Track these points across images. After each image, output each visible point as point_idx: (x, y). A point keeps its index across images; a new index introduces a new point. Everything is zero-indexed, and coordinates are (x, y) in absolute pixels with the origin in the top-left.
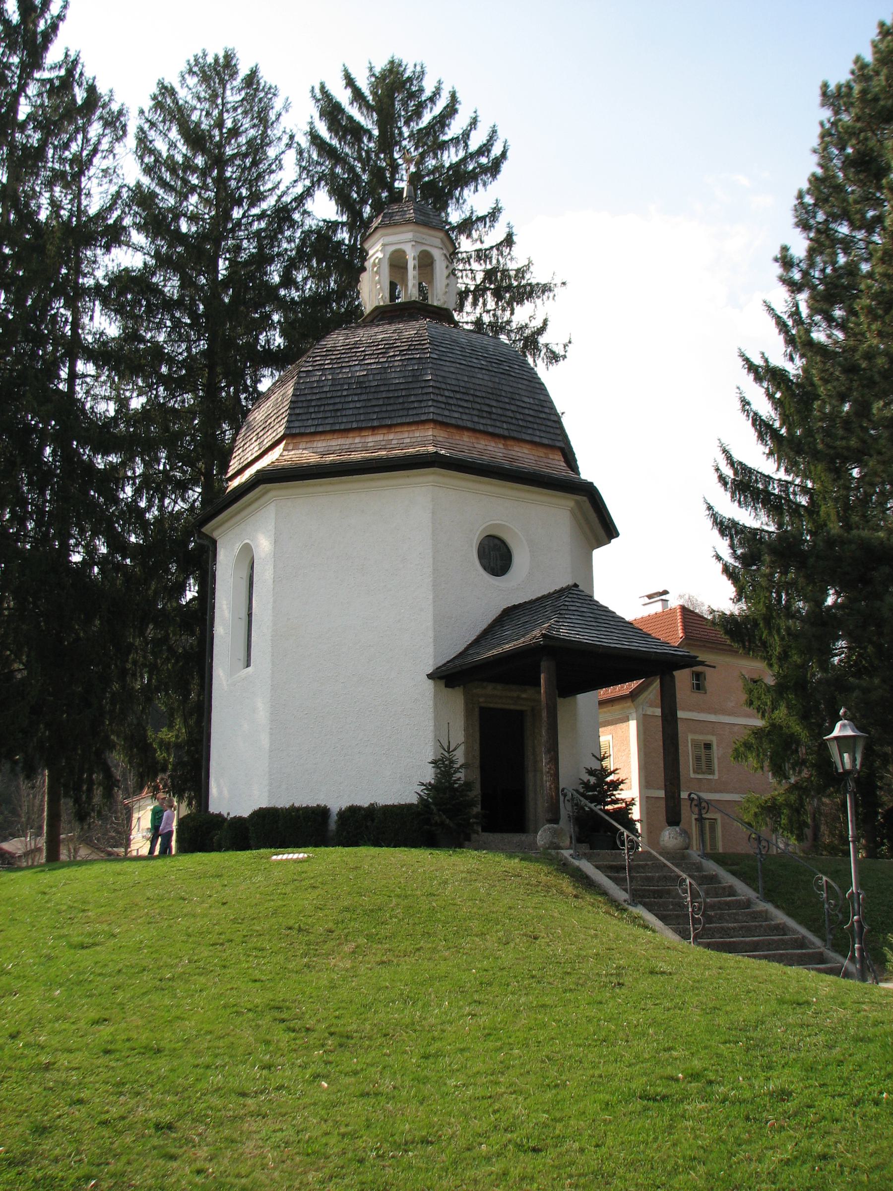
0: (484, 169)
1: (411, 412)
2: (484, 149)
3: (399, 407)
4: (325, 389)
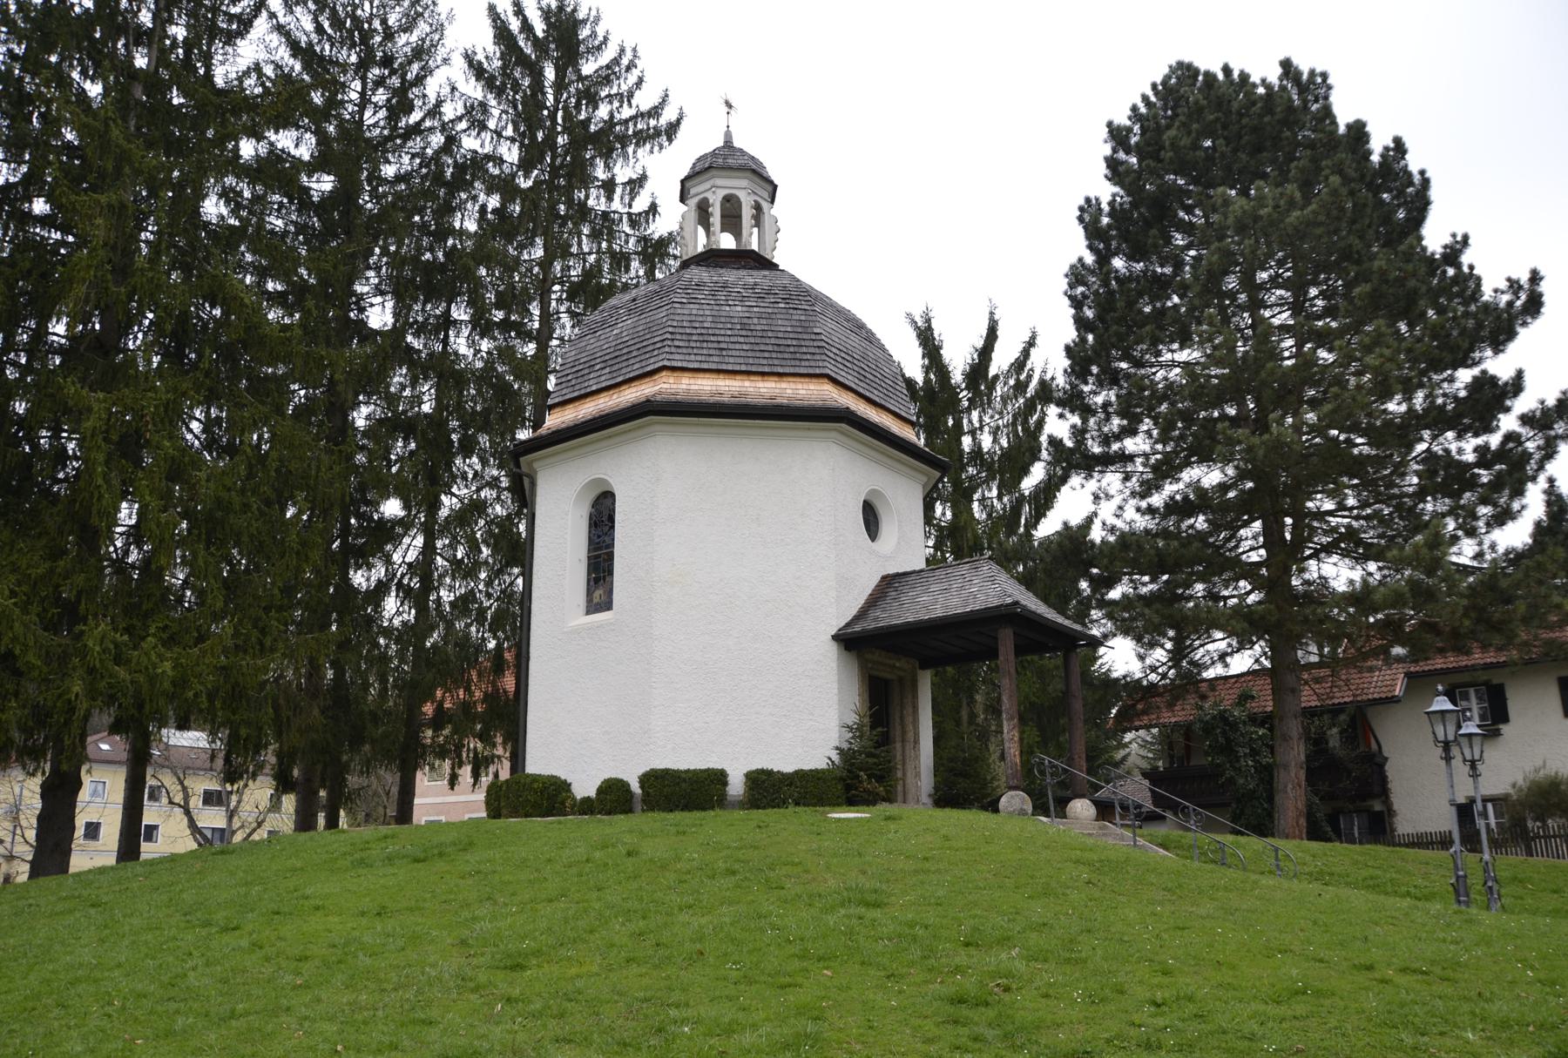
0: (657, 133)
1: (803, 363)
2: (655, 112)
3: (789, 356)
4: (706, 325)
